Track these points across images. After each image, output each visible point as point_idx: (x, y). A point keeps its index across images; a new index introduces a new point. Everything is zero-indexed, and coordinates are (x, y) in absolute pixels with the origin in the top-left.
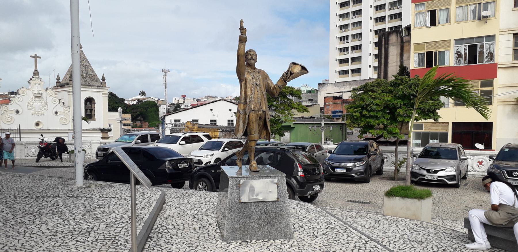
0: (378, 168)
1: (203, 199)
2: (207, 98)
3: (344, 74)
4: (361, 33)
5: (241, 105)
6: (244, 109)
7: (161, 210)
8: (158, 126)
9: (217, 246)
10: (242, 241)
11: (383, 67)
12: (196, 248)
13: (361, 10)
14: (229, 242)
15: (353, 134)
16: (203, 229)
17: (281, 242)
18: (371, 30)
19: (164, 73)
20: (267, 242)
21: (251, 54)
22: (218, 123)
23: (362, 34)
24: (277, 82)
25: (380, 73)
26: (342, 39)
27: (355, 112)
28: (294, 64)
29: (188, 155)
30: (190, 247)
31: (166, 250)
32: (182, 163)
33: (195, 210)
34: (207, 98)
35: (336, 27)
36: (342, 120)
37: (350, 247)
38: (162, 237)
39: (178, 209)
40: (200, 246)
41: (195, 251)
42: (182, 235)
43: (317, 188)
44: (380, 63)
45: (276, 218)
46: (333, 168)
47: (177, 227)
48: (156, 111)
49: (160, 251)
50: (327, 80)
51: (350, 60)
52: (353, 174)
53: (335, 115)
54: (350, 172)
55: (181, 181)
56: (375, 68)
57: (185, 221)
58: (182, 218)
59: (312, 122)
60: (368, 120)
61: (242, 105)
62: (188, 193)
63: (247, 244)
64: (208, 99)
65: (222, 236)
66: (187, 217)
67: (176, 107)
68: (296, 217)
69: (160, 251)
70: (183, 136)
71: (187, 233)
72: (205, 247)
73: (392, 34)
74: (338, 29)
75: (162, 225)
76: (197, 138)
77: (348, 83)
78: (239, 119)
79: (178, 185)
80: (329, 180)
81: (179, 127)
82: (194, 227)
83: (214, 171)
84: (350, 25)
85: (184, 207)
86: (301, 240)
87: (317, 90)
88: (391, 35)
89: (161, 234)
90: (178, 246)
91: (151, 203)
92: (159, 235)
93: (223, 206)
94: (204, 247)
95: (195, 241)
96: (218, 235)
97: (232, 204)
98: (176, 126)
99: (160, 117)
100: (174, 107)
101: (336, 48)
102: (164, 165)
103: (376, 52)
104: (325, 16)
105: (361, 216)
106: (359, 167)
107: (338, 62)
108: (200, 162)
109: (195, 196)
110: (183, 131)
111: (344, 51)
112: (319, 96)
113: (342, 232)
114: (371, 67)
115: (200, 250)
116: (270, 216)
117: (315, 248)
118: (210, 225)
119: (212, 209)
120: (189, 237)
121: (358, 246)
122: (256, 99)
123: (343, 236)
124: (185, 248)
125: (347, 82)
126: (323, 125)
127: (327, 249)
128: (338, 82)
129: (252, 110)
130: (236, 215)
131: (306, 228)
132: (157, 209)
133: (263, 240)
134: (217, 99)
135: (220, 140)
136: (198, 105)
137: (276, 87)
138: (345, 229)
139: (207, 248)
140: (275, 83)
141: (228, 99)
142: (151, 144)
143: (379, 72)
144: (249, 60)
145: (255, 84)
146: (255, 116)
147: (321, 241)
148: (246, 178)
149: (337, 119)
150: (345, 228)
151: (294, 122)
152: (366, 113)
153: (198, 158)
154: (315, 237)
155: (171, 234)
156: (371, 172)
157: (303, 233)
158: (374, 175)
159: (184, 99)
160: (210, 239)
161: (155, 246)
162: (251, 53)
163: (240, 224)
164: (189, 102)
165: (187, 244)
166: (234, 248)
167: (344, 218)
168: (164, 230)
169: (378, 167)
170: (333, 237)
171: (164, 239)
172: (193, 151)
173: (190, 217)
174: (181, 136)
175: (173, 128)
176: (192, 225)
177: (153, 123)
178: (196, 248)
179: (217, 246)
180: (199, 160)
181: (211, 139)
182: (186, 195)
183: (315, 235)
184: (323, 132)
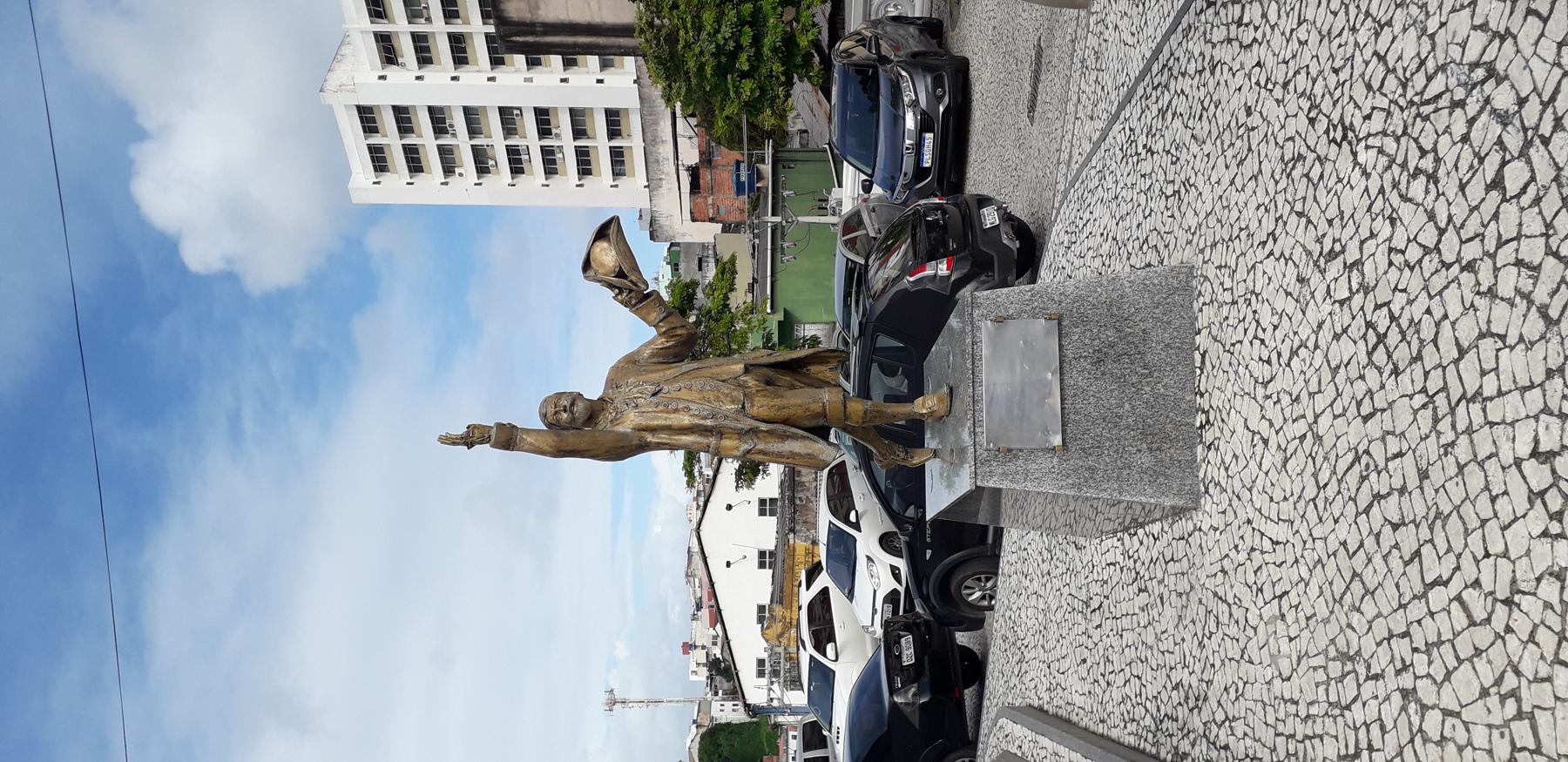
0: (921, 32)
1: (1028, 583)
2: (692, 579)
3: (622, 162)
4: (500, 108)
5: (726, 448)
6: (736, 436)
7: (1069, 721)
8: (777, 726)
9: (1216, 529)
10: (1201, 442)
11: (601, 40)
12: (1225, 601)
13: (431, 110)
14: (1203, 489)
15: (806, 131)
16: (1147, 578)
17: (1204, 304)
18: (491, 79)
19: (618, 706)
20: (1203, 356)
21: (556, 413)
22: (770, 545)
23: (503, 107)
24: (649, 324)
25: (620, 47)
26: (517, 169)
27: (738, 93)
28: (587, 265)
29: (868, 637)
30: (1218, 623)
31: (1230, 704)
32: (900, 654)
33: (1070, 609)
34: (692, 579)
35: (480, 184)
36: (764, 163)
37: (1228, 59)
38: (1176, 720)
39: (1065, 665)
40: (1217, 589)
41: (1235, 603)
42: (1168, 651)
43: (990, 217)
44: (588, 50)
45: (1118, 324)
46: (920, 173)
47: (1138, 669)
48: (730, 733)
49: (1233, 724)
50: (641, 216)
51: (581, 143)
52: (941, 109)
53: (748, 187)
54: (931, 119)
55: (958, 659)
56: (605, 65)
57: (1116, 642)
58: (1101, 652)
59: (769, 252)
60: (766, 50)
61: (727, 443)
62: (1003, 632)
63: (1213, 425)
64: (694, 576)
65: (1178, 513)
66: (1096, 635)
67: (720, 672)
68: (1104, 264)
69: (1233, 724)
70: (811, 650)
71: (1163, 633)
72: (1221, 571)
73: (502, 11)
74: (487, 180)
75: (1127, 719)
76: (818, 608)
77: (651, 148)
78: (773, 453)
79: (974, 668)
80: (958, 186)
81: (779, 663)
82: (1137, 611)
83: (929, 553)
84: (475, 142)
85: (1059, 646)
86: (1201, 236)
87: (672, 245)
88: (506, 15)
89: (1161, 721)
90: (1213, 665)
91: (1043, 753)
92: (1167, 729)
93: (1054, 519)
94: (1219, 573)
95: (1194, 605)
96: (1171, 526)
97: (1068, 476)
98: (775, 673)
99: (748, 719)
100: (718, 678)
101: (543, 185)
102: (908, 710)
103: (556, 60)
104: (446, 219)
105: (1096, 53)
106: (916, 91)
107: (588, 180)
108: (892, 597)
109: (1014, 609)
110: (793, 649)
111: (554, 162)
112: (688, 239)
113: (1167, 97)
114: (600, 77)
115: (1232, 587)
116: (1111, 346)
117: (1232, 183)
118: (1129, 558)
119: (1067, 554)
120: (1177, 626)
121: (1225, 33)
122: (705, 394)
123: (1182, 90)
124: (1223, 639)
125: (648, 152)
126: (778, 219)
127: (1238, 138)
128: (648, 180)
129: (743, 407)
130: (1107, 464)
131: (1147, 225)
132: (1067, 732)
133: (1198, 371)
134: (696, 548)
135: (823, 536)
136: (712, 607)
137: (664, 329)
138: (1155, 88)
139: (1225, 562)
140: (652, 332)
141: (696, 515)
142: (833, 747)
143: (618, 52)
144: (573, 420)
145: (654, 399)
146: (761, 399)
147: (1203, 164)
148: (978, 430)
149: (760, 177)
150: (1149, 90)
151: (769, 311)
152: (743, 57)
153: (879, 606)
154: (1187, 190)
155: (1164, 687)
156: (935, 54)
157: (1168, 233)
158: (940, 45)
159: (696, 647)
160: (1187, 555)
161: (1214, 744)
162: (551, 410)
163: (1140, 451)
164: (703, 632)
165: (1207, 632)
166: (1227, 469)
167: (1106, 108)
168: (1147, 710)
169: (917, 32)
170: (1186, 127)
171: (1182, 713)
172: (856, 620)
173: (1099, 626)
174: (811, 656)
175: (782, 680)
176: (1129, 617)
177: (764, 739)
178: (1225, 601)
179: (1216, 529)
180: (887, 600)
181: (820, 563)
182: (1012, 640)
183: (1179, 192)
184: (801, 219)
